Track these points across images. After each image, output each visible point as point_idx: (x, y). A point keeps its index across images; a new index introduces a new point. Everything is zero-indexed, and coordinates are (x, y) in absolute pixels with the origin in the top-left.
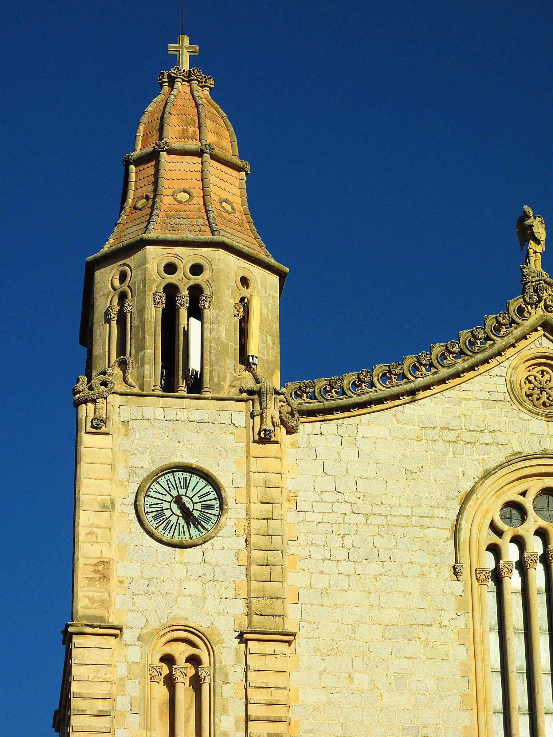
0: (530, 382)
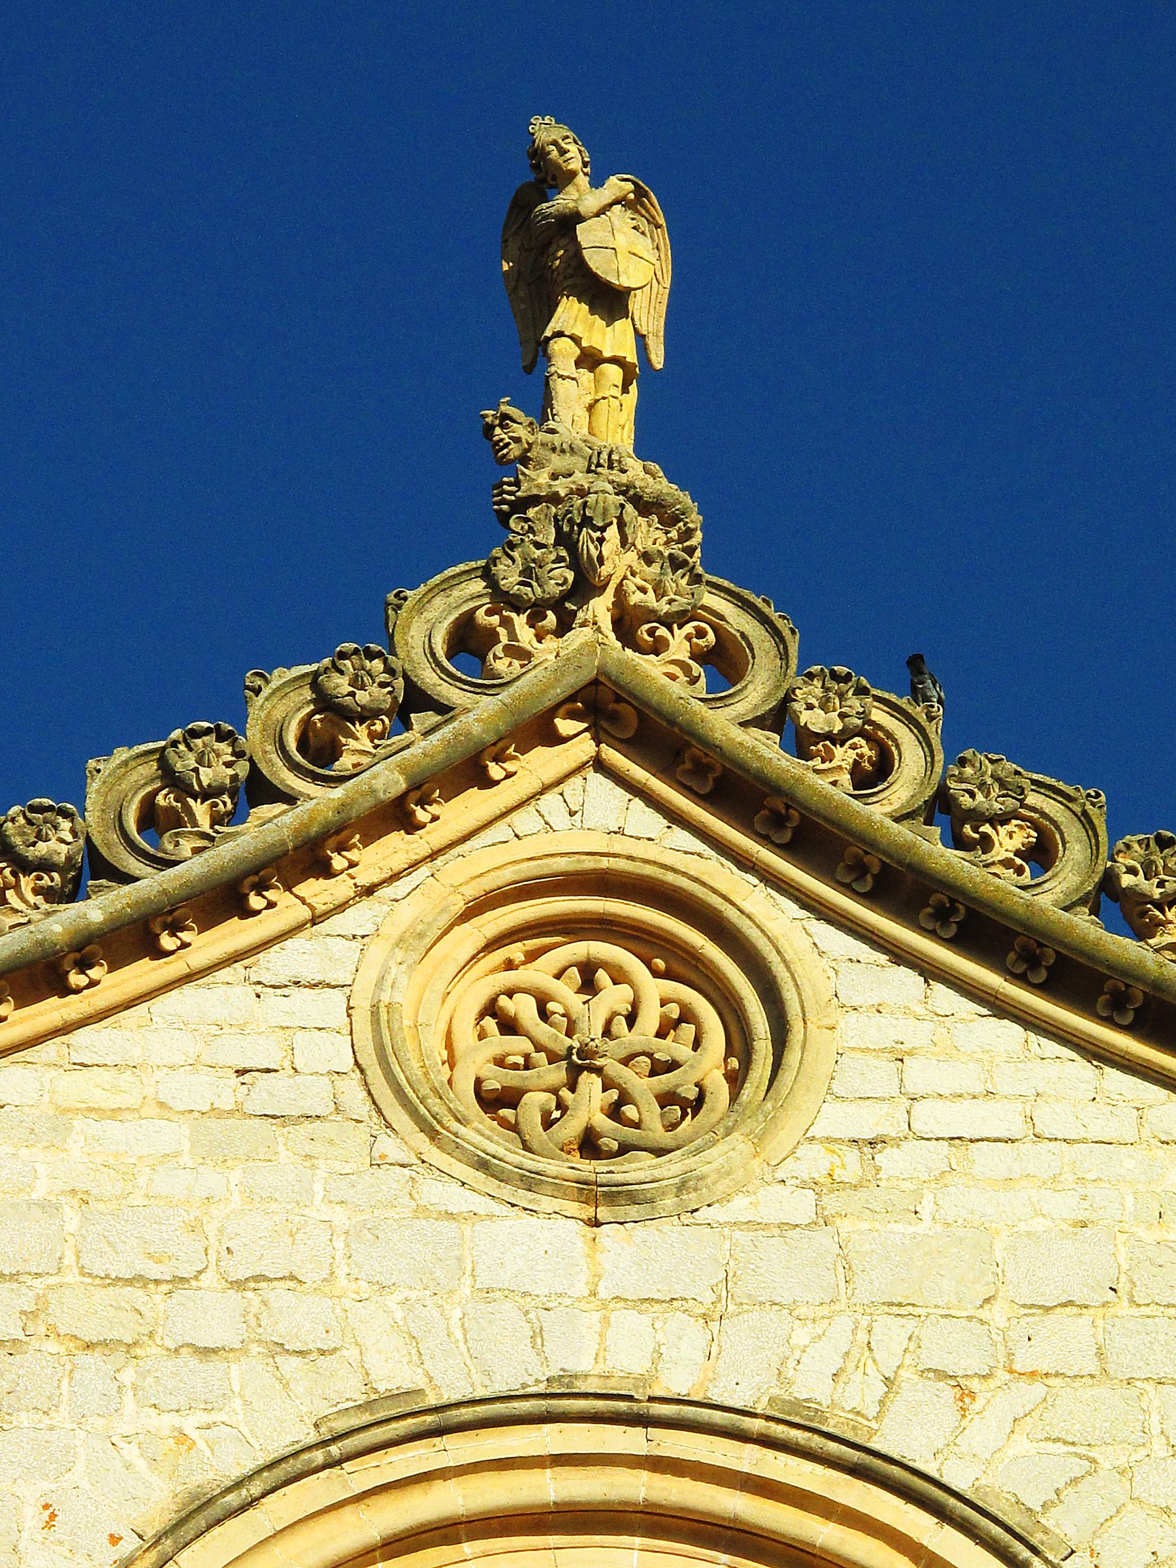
0: (509, 1026)
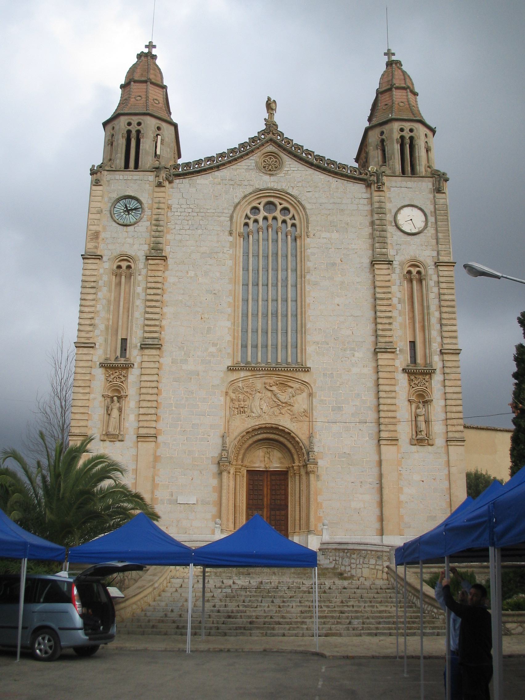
0: (265, 162)
